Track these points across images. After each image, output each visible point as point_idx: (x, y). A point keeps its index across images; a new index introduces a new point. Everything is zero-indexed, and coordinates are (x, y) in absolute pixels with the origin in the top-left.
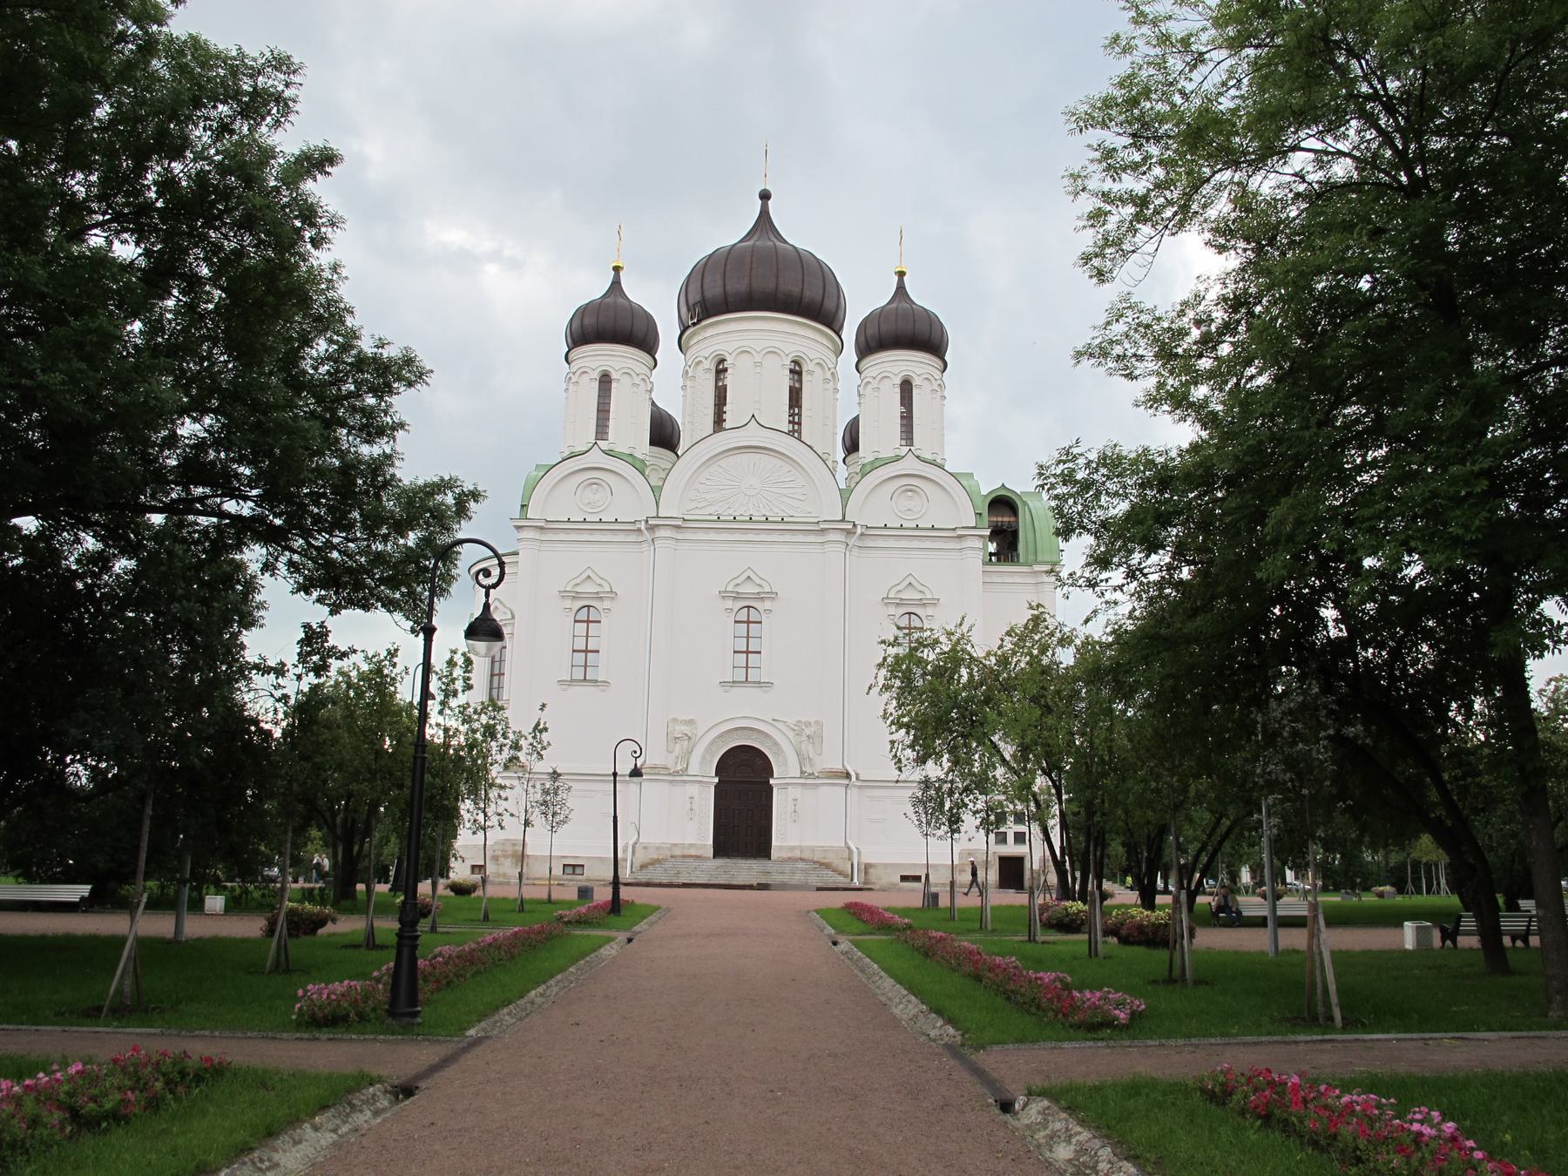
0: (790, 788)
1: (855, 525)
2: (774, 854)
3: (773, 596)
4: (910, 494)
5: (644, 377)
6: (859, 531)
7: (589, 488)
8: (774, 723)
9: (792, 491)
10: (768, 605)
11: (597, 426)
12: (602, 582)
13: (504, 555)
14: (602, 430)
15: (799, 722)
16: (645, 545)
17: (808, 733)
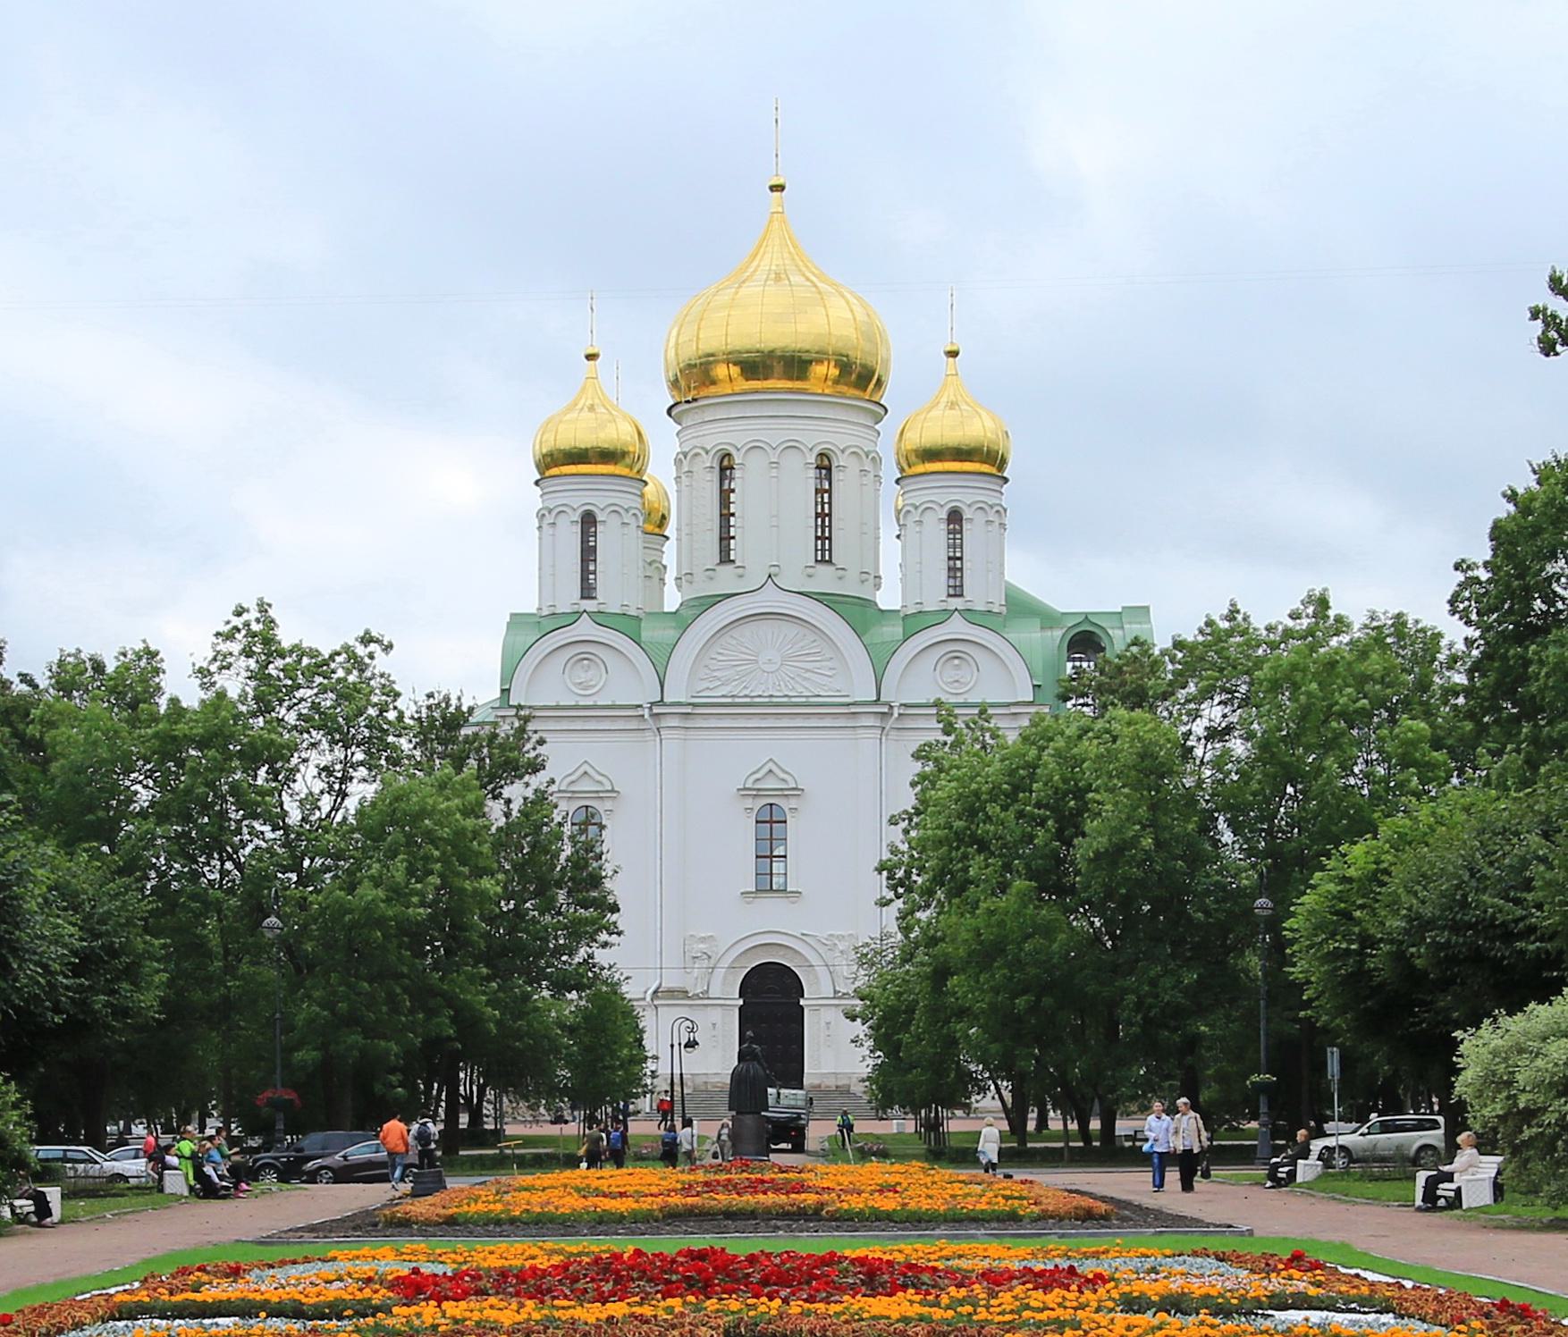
0: (822, 1009)
1: (891, 707)
2: (806, 1082)
3: (797, 791)
4: (956, 662)
5: (636, 511)
6: (896, 712)
7: (580, 664)
8: (804, 938)
9: (818, 664)
10: (793, 803)
11: (582, 589)
12: (600, 778)
13: (1002, 1118)
14: (587, 591)
15: (831, 935)
16: (647, 734)
17: (841, 948)
